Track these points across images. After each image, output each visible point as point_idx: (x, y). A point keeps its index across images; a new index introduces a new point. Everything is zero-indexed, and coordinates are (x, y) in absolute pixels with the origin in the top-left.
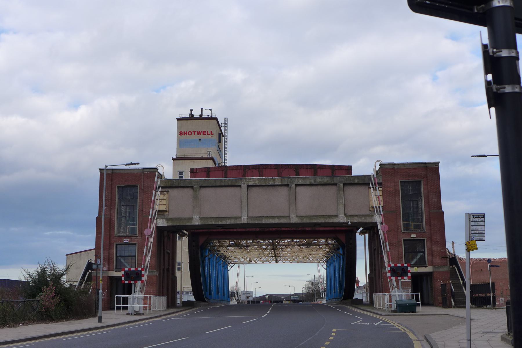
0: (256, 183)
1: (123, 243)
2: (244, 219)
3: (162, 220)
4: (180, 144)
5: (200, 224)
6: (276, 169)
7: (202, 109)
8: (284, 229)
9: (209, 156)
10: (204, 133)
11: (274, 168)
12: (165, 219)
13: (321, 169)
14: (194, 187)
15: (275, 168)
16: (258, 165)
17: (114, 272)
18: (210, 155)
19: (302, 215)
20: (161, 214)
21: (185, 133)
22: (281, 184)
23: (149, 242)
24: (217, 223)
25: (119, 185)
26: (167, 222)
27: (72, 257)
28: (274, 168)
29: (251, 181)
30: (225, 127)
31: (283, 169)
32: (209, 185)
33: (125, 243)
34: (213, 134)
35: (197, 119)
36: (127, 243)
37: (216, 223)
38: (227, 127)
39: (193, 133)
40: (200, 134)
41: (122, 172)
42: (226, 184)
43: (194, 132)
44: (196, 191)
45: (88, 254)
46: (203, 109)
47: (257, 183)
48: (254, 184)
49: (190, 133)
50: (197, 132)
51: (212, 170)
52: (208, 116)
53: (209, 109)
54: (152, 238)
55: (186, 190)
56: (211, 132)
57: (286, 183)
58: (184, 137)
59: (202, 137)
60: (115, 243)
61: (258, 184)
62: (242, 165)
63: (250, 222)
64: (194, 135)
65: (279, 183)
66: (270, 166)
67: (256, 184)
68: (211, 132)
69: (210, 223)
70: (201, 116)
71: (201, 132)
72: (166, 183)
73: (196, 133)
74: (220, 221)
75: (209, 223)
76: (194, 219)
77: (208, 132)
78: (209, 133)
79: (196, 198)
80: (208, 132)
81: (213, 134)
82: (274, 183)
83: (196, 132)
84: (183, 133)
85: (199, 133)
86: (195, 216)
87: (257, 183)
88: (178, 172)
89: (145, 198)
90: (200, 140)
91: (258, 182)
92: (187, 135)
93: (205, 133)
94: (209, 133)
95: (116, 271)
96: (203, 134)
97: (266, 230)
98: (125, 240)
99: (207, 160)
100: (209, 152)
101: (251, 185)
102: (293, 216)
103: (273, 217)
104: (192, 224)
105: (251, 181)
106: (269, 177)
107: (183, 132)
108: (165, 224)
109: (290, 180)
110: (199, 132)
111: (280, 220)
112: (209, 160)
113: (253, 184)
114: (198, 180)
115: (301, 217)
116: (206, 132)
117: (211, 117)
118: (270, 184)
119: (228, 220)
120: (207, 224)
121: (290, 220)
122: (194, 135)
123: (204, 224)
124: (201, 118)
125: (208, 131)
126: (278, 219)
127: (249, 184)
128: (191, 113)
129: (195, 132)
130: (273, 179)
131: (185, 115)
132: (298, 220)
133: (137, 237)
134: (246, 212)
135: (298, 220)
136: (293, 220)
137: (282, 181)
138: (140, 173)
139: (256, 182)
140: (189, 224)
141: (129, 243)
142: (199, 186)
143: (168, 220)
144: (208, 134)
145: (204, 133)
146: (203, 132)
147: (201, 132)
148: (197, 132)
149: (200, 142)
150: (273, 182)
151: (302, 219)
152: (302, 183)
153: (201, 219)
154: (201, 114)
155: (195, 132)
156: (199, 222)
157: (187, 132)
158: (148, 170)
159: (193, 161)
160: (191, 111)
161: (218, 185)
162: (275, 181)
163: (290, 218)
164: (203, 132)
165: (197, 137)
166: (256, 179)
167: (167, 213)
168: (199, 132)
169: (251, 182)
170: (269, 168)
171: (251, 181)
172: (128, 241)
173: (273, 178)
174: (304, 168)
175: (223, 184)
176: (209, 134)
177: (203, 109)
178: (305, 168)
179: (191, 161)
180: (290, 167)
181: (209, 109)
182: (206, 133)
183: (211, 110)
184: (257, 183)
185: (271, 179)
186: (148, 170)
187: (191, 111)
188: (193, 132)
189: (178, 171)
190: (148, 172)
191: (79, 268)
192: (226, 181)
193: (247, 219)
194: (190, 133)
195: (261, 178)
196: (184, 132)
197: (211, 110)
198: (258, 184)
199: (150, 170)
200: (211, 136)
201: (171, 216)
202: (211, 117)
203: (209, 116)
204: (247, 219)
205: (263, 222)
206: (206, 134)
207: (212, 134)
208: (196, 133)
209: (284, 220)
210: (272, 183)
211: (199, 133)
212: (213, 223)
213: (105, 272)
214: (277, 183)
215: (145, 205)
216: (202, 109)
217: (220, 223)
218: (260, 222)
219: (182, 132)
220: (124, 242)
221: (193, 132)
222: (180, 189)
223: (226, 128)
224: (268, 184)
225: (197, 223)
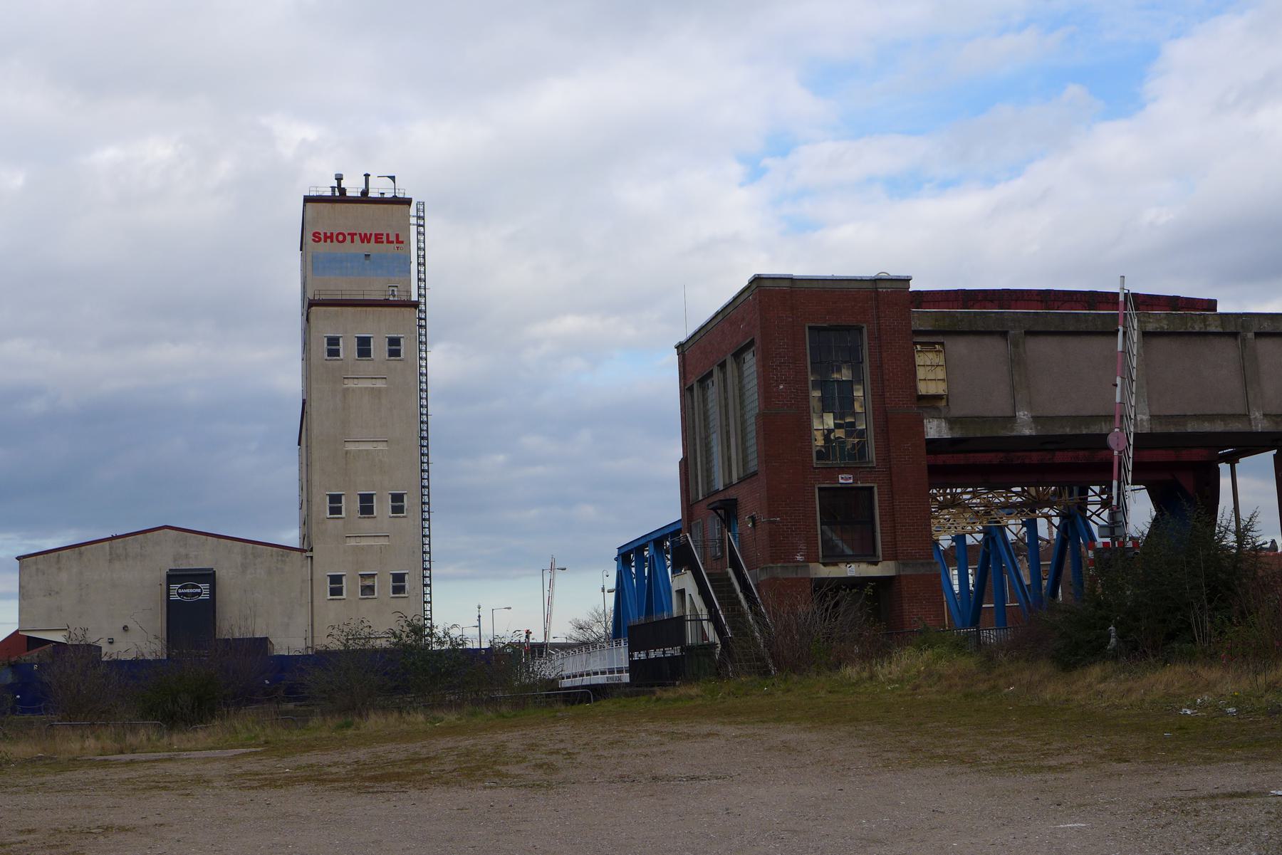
0: (1163, 328)
1: (839, 485)
2: (1141, 420)
3: (935, 422)
4: (311, 266)
5: (1034, 434)
6: (1042, 301)
7: (367, 176)
8: (1060, 457)
9: (391, 298)
10: (378, 238)
11: (1038, 301)
12: (946, 418)
13: (1147, 305)
14: (1012, 332)
15: (1040, 299)
16: (994, 291)
17: (821, 566)
18: (394, 296)
19: (1274, 413)
20: (926, 407)
21: (329, 237)
22: (1221, 330)
23: (1123, 470)
24: (1078, 432)
25: (813, 324)
26: (951, 429)
27: (36, 563)
28: (1038, 301)
29: (1151, 320)
30: (419, 225)
31: (1060, 303)
32: (1049, 329)
33: (843, 486)
34: (402, 242)
35: (354, 200)
36: (850, 486)
37: (1073, 432)
38: (423, 226)
39: (349, 238)
40: (369, 242)
41: (816, 286)
42: (1091, 328)
43: (352, 235)
44: (1016, 345)
45: (81, 554)
46: (369, 175)
47: (1165, 326)
48: (1159, 330)
49: (341, 238)
50: (360, 234)
51: (925, 300)
52: (381, 194)
53: (388, 177)
54: (1129, 458)
55: (988, 341)
56: (397, 236)
57: (1232, 329)
58: (324, 247)
59: (372, 247)
60: (817, 486)
61: (1167, 329)
62: (958, 290)
63: (1158, 429)
64: (352, 241)
65: (1217, 327)
66: (1028, 295)
67: (1162, 330)
68: (397, 236)
69: (1059, 432)
70: (365, 193)
71: (371, 235)
72: (936, 320)
73: (357, 238)
74: (1083, 427)
75: (1058, 430)
76: (1019, 421)
77: (388, 235)
78: (392, 238)
79: (1016, 363)
80: (388, 235)
81: (402, 242)
82: (1206, 328)
83: (358, 235)
84: (322, 236)
85: (365, 238)
86: (1021, 413)
87: (1166, 327)
88: (326, 339)
89: (886, 361)
90: (367, 256)
91: (1168, 325)
92: (332, 241)
93: (382, 238)
94: (392, 238)
95: (825, 565)
96: (376, 242)
97: (1016, 462)
98: (843, 476)
99: (403, 309)
100: (393, 288)
101: (1151, 330)
102: (1256, 414)
103: (1211, 418)
104: (1014, 433)
105: (1150, 322)
106: (1193, 312)
107: (385, 235)
108: (946, 434)
109: (1241, 320)
110: (366, 235)
111: (1229, 424)
112: (408, 309)
113: (1157, 328)
114: (1019, 314)
115: (1273, 418)
116: (382, 235)
117: (395, 196)
118: (1197, 329)
119: (1103, 424)
120: (1051, 433)
121: (1250, 424)
122: (352, 241)
123: (1044, 432)
124: (364, 198)
125: (390, 232)
126: (1222, 423)
127: (1147, 330)
128: (339, 184)
129: (356, 234)
130: (1202, 316)
131: (323, 189)
132: (1267, 425)
133: (874, 467)
134: (1144, 401)
135: (1267, 425)
136: (1257, 426)
137: (1222, 323)
138: (867, 291)
139: (1162, 325)
140: (1009, 434)
141: (854, 485)
142: (1023, 331)
143: (952, 422)
144: (389, 242)
145: (378, 238)
146: (376, 235)
147: (371, 235)
148: (360, 234)
149: (368, 262)
150: (1202, 326)
151: (1277, 423)
152: (1270, 331)
153: (1036, 419)
154: (364, 187)
155: (356, 234)
156: (1031, 429)
157: (332, 234)
158: (888, 284)
159: (364, 309)
160: (339, 178)
161: (1071, 329)
162: (1207, 323)
163: (1250, 420)
164: (376, 235)
165: (359, 248)
166: (1162, 315)
167: (943, 403)
168: (366, 235)
169: (1151, 325)
170: (1025, 300)
171: (1151, 320)
172: (851, 481)
173: (1201, 314)
174: (1108, 303)
175: (1083, 327)
176: (392, 242)
177: (369, 175)
178: (1111, 301)
179: (359, 309)
180: (1075, 298)
181: (388, 177)
182: (384, 238)
183: (393, 178)
184: (1166, 327)
185: (1198, 317)
186: (888, 284)
187: (339, 178)
188: (349, 234)
189: (325, 335)
190: (889, 290)
191: (57, 593)
192: (1090, 318)
193: (1151, 420)
194: (341, 238)
195: (1174, 312)
196: (325, 234)
197: (393, 178)
198: (1169, 330)
199: (895, 285)
200: (398, 248)
201: (955, 412)
202: (395, 196)
203: (383, 194)
204: (1149, 423)
205: (1189, 430)
206: (382, 242)
207: (398, 242)
208: (357, 238)
209: (1237, 424)
210: (1201, 328)
211: (365, 238)
212: (1068, 431)
213: (802, 566)
214: (1212, 329)
215: (888, 380)
216: (367, 176)
217: (1084, 432)
218: (1181, 429)
219: (320, 234)
220: (841, 481)
221: (349, 234)
222: (972, 339)
223: (421, 229)
224: (1190, 330)
225: (1027, 432)
